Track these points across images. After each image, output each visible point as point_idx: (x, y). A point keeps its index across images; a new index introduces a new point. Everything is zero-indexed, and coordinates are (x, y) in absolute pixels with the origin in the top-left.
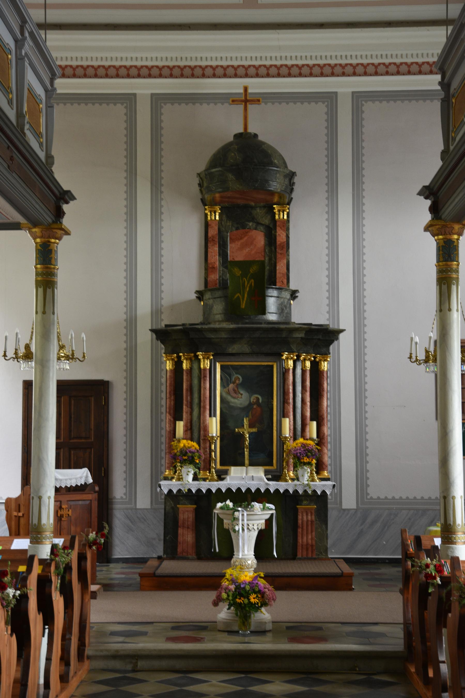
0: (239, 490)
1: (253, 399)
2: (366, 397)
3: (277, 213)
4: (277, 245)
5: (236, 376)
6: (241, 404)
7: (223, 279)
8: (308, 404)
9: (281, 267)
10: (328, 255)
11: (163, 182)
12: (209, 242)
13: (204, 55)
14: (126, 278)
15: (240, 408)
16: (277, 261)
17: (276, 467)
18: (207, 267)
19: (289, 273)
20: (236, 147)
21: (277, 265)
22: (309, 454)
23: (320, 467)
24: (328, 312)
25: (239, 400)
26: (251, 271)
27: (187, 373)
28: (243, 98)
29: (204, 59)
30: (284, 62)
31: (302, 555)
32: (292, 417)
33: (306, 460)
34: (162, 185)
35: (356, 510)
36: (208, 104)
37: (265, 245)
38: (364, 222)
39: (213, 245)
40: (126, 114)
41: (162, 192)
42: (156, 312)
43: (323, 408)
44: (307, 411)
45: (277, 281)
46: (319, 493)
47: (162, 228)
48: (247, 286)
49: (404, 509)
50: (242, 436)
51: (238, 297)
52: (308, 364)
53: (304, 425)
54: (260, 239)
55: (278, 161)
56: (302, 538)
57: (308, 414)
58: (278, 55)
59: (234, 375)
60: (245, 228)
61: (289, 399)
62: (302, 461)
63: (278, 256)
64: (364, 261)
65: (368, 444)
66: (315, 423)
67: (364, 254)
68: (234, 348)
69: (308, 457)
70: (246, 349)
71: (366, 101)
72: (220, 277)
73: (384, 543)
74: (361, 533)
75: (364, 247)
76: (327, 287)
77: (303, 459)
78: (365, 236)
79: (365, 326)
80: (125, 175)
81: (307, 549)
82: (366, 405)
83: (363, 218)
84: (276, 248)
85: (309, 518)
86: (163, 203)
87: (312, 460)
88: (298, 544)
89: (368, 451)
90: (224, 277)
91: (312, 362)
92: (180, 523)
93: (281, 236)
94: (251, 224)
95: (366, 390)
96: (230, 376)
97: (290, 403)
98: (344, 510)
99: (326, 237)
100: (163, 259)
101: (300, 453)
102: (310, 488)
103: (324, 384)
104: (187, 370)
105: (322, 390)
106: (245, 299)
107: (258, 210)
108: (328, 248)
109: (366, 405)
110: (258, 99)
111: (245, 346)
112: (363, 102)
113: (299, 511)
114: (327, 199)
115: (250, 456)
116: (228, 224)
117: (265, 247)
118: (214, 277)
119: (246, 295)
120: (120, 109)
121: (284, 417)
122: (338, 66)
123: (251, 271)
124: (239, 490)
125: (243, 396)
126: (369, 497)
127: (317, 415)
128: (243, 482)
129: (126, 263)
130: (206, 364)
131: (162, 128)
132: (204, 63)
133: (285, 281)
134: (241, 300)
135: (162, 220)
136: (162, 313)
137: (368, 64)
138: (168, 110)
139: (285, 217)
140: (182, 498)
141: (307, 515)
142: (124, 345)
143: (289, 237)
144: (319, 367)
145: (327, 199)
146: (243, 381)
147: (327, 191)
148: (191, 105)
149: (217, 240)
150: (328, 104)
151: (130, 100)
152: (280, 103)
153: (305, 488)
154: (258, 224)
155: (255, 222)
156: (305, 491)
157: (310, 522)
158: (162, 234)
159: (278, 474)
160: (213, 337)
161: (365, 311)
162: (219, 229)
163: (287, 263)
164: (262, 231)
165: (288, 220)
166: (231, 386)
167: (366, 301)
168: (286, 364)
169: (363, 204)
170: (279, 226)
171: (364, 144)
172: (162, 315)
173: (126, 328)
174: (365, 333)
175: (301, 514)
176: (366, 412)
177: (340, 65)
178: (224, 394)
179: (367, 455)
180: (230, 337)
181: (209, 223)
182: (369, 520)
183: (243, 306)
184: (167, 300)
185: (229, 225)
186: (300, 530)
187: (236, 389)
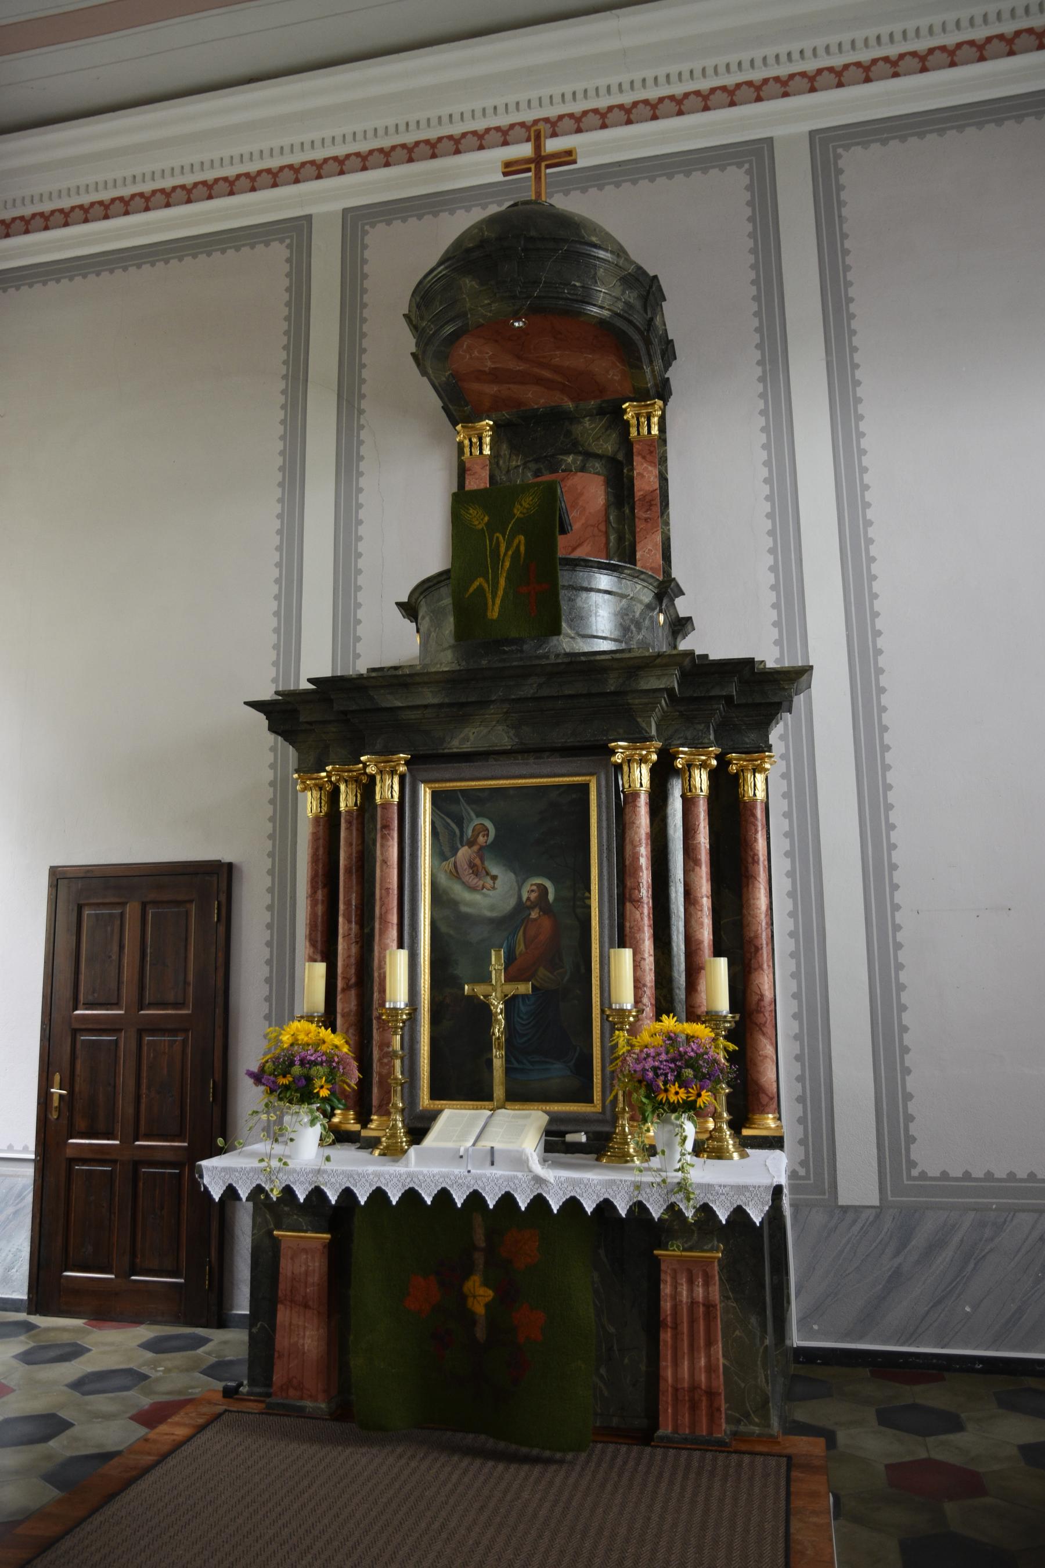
0: (444, 1196)
2: (895, 887)
3: (634, 422)
5: (477, 821)
6: (492, 908)
8: (706, 903)
11: (365, 389)
14: (277, 614)
15: (491, 921)
17: (598, 1108)
22: (689, 1073)
23: (746, 1102)
25: (485, 895)
26: (517, 512)
27: (349, 823)
29: (456, 117)
31: (675, 1430)
32: (648, 945)
33: (676, 1094)
34: (362, 396)
35: (880, 1211)
37: (607, 506)
38: (863, 426)
41: (361, 412)
43: (755, 917)
44: (702, 924)
46: (723, 1217)
47: (360, 490)
48: (505, 554)
49: (1024, 1211)
50: (482, 1011)
51: (480, 588)
52: (701, 780)
53: (694, 970)
56: (676, 1364)
57: (706, 934)
59: (471, 820)
60: (555, 471)
61: (638, 887)
62: (662, 1096)
63: (640, 525)
64: (868, 523)
65: (907, 1018)
66: (722, 963)
67: (867, 505)
68: (468, 738)
69: (684, 1084)
70: (503, 738)
71: (847, 148)
73: (968, 1309)
74: (896, 1279)
75: (866, 488)
77: (666, 1091)
78: (866, 461)
79: (882, 690)
80: (282, 385)
81: (694, 1407)
82: (896, 907)
85: (700, 1292)
86: (364, 435)
87: (699, 1095)
88: (662, 1386)
89: (908, 1039)
91: (713, 775)
92: (283, 1286)
93: (645, 477)
94: (570, 459)
95: (893, 867)
96: (460, 822)
97: (640, 900)
98: (845, 1209)
100: (361, 563)
101: (655, 1069)
102: (689, 1199)
103: (756, 840)
104: (349, 812)
105: (750, 860)
106: (500, 593)
107: (587, 423)
109: (896, 907)
111: (500, 728)
113: (663, 1267)
114: (762, 379)
115: (508, 1071)
116: (514, 463)
117: (606, 510)
119: (502, 582)
121: (622, 944)
123: (515, 511)
124: (444, 1196)
125: (498, 882)
126: (915, 1173)
127: (737, 940)
128: (458, 1171)
129: (278, 581)
130: (388, 790)
134: (489, 596)
135: (360, 474)
139: (655, 431)
140: (286, 1209)
141: (691, 1282)
142: (269, 775)
144: (741, 790)
146: (496, 837)
153: (673, 1199)
154: (589, 455)
155: (580, 453)
156: (672, 1208)
157: (701, 1309)
158: (360, 506)
159: (606, 1129)
160: (399, 704)
161: (879, 652)
162: (492, 477)
163: (663, 544)
164: (598, 474)
166: (464, 853)
168: (626, 778)
170: (639, 454)
175: (669, 1279)
176: (897, 928)
178: (443, 880)
179: (905, 1050)
180: (447, 700)
183: (494, 613)
185: (518, 467)
186: (666, 1336)
187: (477, 861)
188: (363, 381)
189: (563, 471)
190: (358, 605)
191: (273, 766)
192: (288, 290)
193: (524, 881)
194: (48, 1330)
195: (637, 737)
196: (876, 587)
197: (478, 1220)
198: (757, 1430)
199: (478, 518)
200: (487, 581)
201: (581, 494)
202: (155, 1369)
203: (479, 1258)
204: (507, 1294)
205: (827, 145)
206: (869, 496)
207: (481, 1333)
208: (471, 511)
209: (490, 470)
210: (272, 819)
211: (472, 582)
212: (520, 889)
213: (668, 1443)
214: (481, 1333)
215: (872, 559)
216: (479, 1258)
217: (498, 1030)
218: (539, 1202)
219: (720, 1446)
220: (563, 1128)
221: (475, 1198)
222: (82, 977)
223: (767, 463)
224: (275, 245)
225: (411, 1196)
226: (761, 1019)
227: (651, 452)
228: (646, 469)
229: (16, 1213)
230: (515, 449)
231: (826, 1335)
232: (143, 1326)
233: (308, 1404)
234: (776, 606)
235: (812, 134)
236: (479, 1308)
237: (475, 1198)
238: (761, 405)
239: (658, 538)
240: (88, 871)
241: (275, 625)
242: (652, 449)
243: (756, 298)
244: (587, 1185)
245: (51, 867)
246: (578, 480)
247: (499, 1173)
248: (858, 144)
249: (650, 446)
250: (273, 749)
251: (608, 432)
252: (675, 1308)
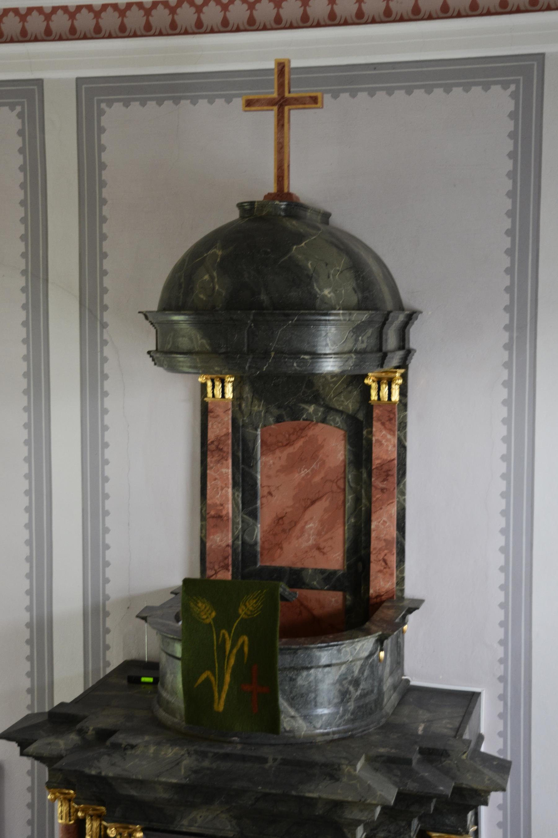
4: (374, 467)
7: (243, 542)
9: (382, 525)
11: (107, 299)
12: (209, 453)
16: (373, 509)
18: (207, 516)
21: (374, 517)
26: (242, 611)
28: (275, 95)
34: (105, 308)
39: (218, 462)
40: (21, 133)
41: (104, 325)
42: (95, 614)
45: (373, 557)
51: (207, 680)
54: (334, 446)
55: (335, 291)
60: (298, 419)
63: (376, 495)
72: (235, 539)
76: (500, 578)
84: (370, 476)
86: (108, 351)
90: (247, 538)
93: (383, 446)
94: (311, 409)
106: (226, 687)
111: (224, 816)
118: (222, 539)
123: (240, 611)
131: (103, 166)
133: (393, 559)
134: (216, 689)
135: (105, 394)
136: (106, 614)
139: (396, 397)
142: (27, 683)
150: (518, 88)
152: (390, 91)
154: (329, 409)
155: (322, 406)
162: (234, 421)
163: (398, 514)
164: (338, 427)
165: (403, 404)
170: (379, 420)
173: (29, 642)
181: (210, 406)
183: (220, 706)
184: (116, 588)
188: (104, 291)
189: (304, 420)
192: (22, 168)
199: (206, 613)
200: (214, 674)
201: (322, 447)
208: (200, 605)
209: (233, 412)
211: (200, 674)
223: (506, 440)
227: (390, 420)
228: (384, 437)
230: (258, 393)
239: (394, 510)
241: (27, 570)
242: (392, 416)
243: (510, 252)
249: (390, 412)
250: (30, 773)
251: (350, 388)
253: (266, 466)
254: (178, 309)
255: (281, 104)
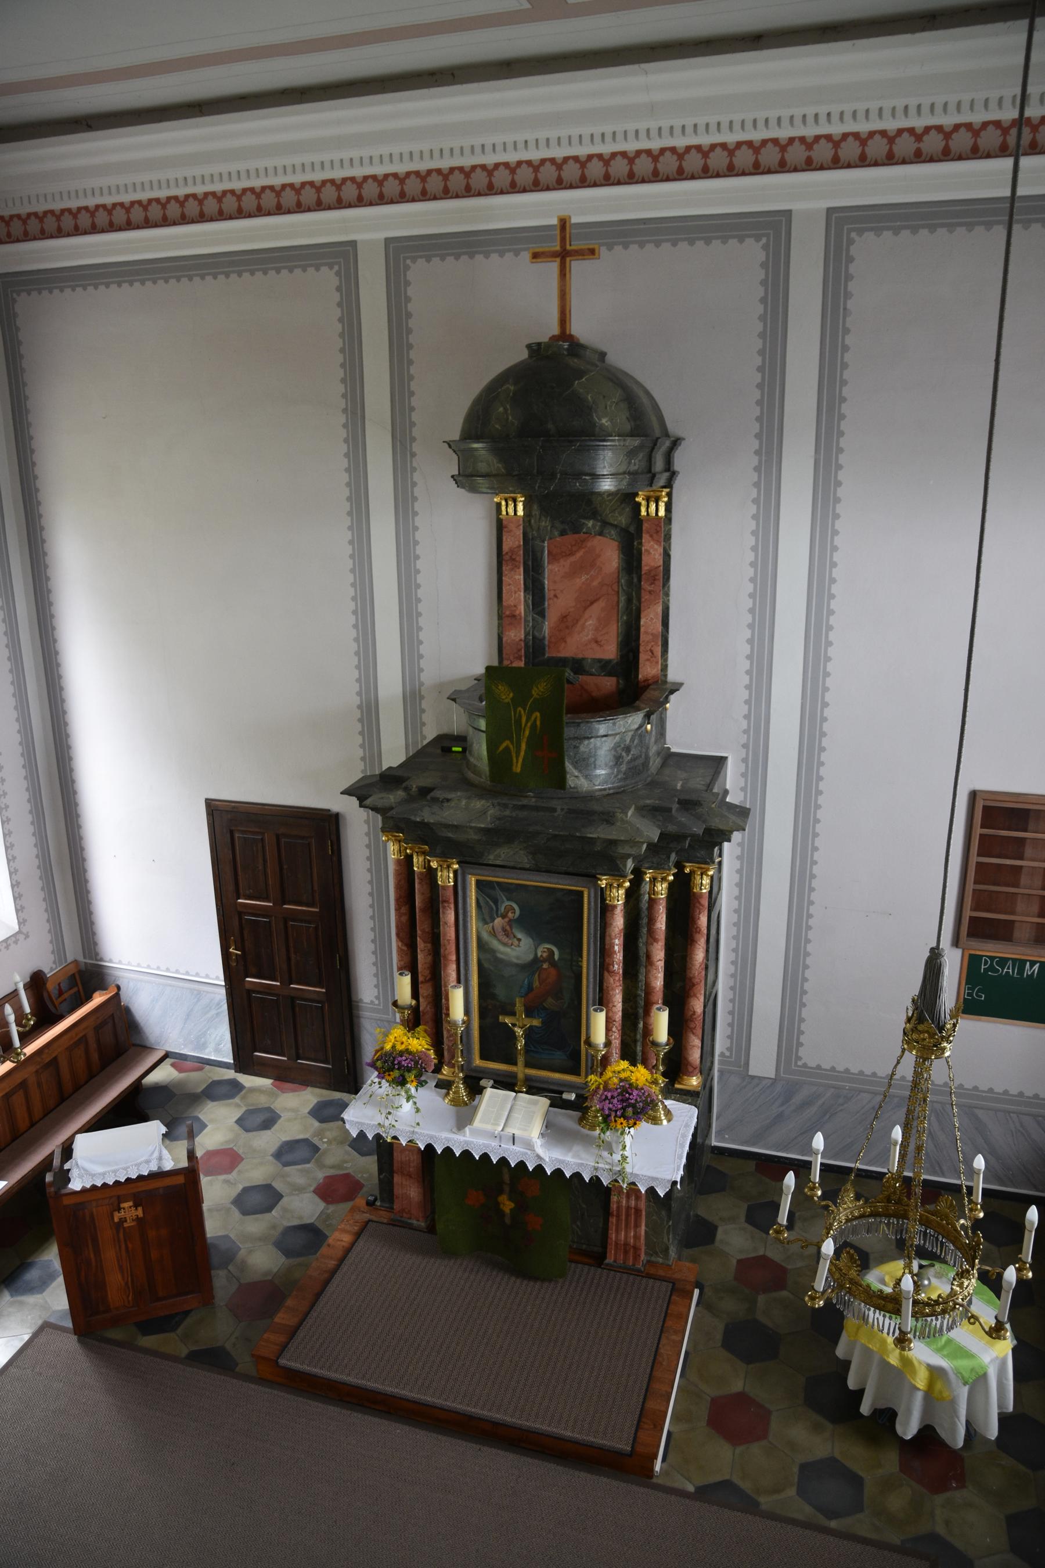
0: (485, 1157)
1: (543, 950)
5: (508, 903)
6: (518, 958)
7: (534, 637)
9: (649, 621)
10: (752, 596)
13: (488, 140)
15: (517, 965)
16: (642, 608)
18: (503, 616)
19: (667, 631)
20: (512, 388)
24: (747, 717)
28: (558, 248)
29: (488, 148)
30: (668, 142)
31: (615, 1261)
34: (413, 439)
35: (774, 1081)
36: (502, 254)
39: (512, 570)
45: (642, 649)
51: (507, 748)
54: (609, 555)
55: (611, 420)
56: (617, 1232)
58: (653, 125)
63: (645, 596)
64: (831, 612)
67: (832, 597)
68: (502, 854)
71: (861, 232)
72: (527, 634)
74: (779, 1118)
75: (833, 581)
79: (822, 749)
81: (626, 1252)
83: (837, 516)
84: (640, 581)
85: (633, 1203)
86: (416, 477)
90: (537, 634)
93: (651, 554)
94: (590, 523)
96: (496, 902)
98: (753, 1077)
99: (750, 556)
106: (522, 753)
108: (753, 580)
110: (591, 247)
111: (522, 852)
112: (853, 235)
118: (516, 635)
119: (523, 746)
120: (327, 278)
122: (797, 143)
124: (485, 1157)
127: (677, 998)
132: (490, 159)
133: (658, 650)
134: (514, 755)
136: (422, 698)
137: (872, 134)
138: (418, 271)
139: (662, 513)
142: (360, 753)
143: (669, 556)
145: (757, 469)
147: (757, 453)
148: (464, 258)
149: (520, 558)
151: (343, 256)
154: (605, 524)
161: (824, 719)
162: (525, 534)
163: (663, 612)
165: (668, 518)
166: (498, 921)
167: (828, 697)
169: (839, 484)
170: (648, 532)
171: (848, 340)
172: (423, 702)
174: (821, 764)
177: (802, 139)
178: (485, 936)
181: (504, 522)
182: (797, 1099)
183: (517, 768)
186: (613, 1220)
187: (508, 928)
188: (413, 424)
190: (420, 629)
191: (362, 746)
193: (539, 945)
194: (252, 1090)
195: (617, 873)
196: (830, 667)
197: (505, 1170)
198: (661, 1260)
199: (505, 694)
200: (512, 743)
201: (599, 556)
202: (321, 1139)
203: (507, 1188)
204: (522, 1206)
205: (843, 224)
206: (834, 589)
207: (508, 1221)
210: (358, 667)
212: (536, 949)
213: (610, 1268)
214: (508, 1221)
215: (829, 644)
216: (507, 1188)
217: (520, 1044)
218: (540, 1168)
219: (638, 1273)
220: (561, 1089)
221: (503, 1161)
222: (240, 878)
223: (754, 549)
224: (324, 269)
225: (466, 1154)
226: (692, 1025)
228: (652, 547)
229: (217, 1014)
231: (733, 1142)
232: (309, 1089)
233: (415, 1222)
234: (749, 672)
235: (830, 211)
236: (507, 1210)
237: (503, 1161)
238: (754, 493)
239: (659, 609)
240: (234, 807)
244: (568, 1164)
245: (206, 800)
246: (597, 542)
247: (518, 1149)
248: (871, 229)
252: (619, 1208)
253: (552, 573)
254: (478, 438)
255: (564, 256)
